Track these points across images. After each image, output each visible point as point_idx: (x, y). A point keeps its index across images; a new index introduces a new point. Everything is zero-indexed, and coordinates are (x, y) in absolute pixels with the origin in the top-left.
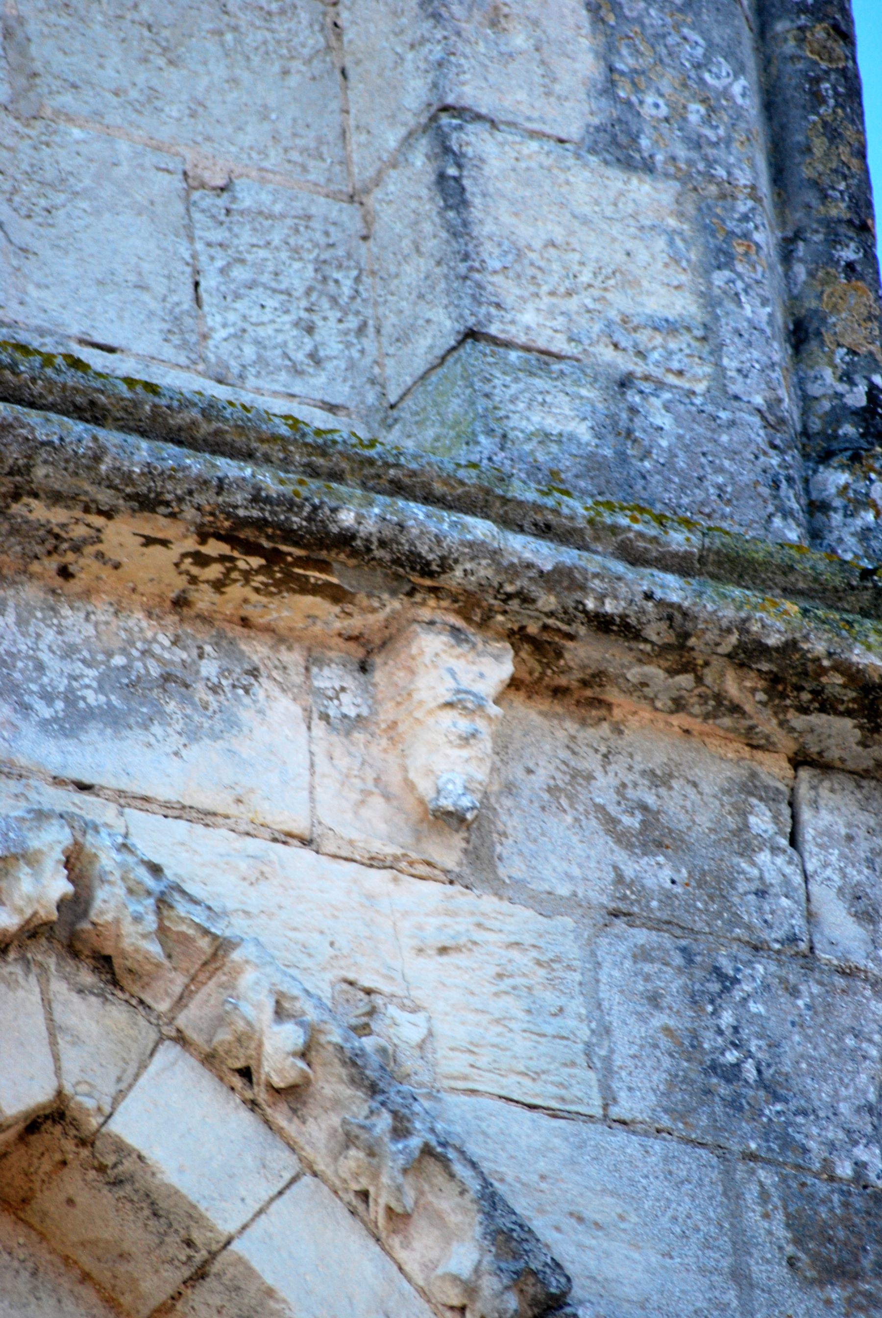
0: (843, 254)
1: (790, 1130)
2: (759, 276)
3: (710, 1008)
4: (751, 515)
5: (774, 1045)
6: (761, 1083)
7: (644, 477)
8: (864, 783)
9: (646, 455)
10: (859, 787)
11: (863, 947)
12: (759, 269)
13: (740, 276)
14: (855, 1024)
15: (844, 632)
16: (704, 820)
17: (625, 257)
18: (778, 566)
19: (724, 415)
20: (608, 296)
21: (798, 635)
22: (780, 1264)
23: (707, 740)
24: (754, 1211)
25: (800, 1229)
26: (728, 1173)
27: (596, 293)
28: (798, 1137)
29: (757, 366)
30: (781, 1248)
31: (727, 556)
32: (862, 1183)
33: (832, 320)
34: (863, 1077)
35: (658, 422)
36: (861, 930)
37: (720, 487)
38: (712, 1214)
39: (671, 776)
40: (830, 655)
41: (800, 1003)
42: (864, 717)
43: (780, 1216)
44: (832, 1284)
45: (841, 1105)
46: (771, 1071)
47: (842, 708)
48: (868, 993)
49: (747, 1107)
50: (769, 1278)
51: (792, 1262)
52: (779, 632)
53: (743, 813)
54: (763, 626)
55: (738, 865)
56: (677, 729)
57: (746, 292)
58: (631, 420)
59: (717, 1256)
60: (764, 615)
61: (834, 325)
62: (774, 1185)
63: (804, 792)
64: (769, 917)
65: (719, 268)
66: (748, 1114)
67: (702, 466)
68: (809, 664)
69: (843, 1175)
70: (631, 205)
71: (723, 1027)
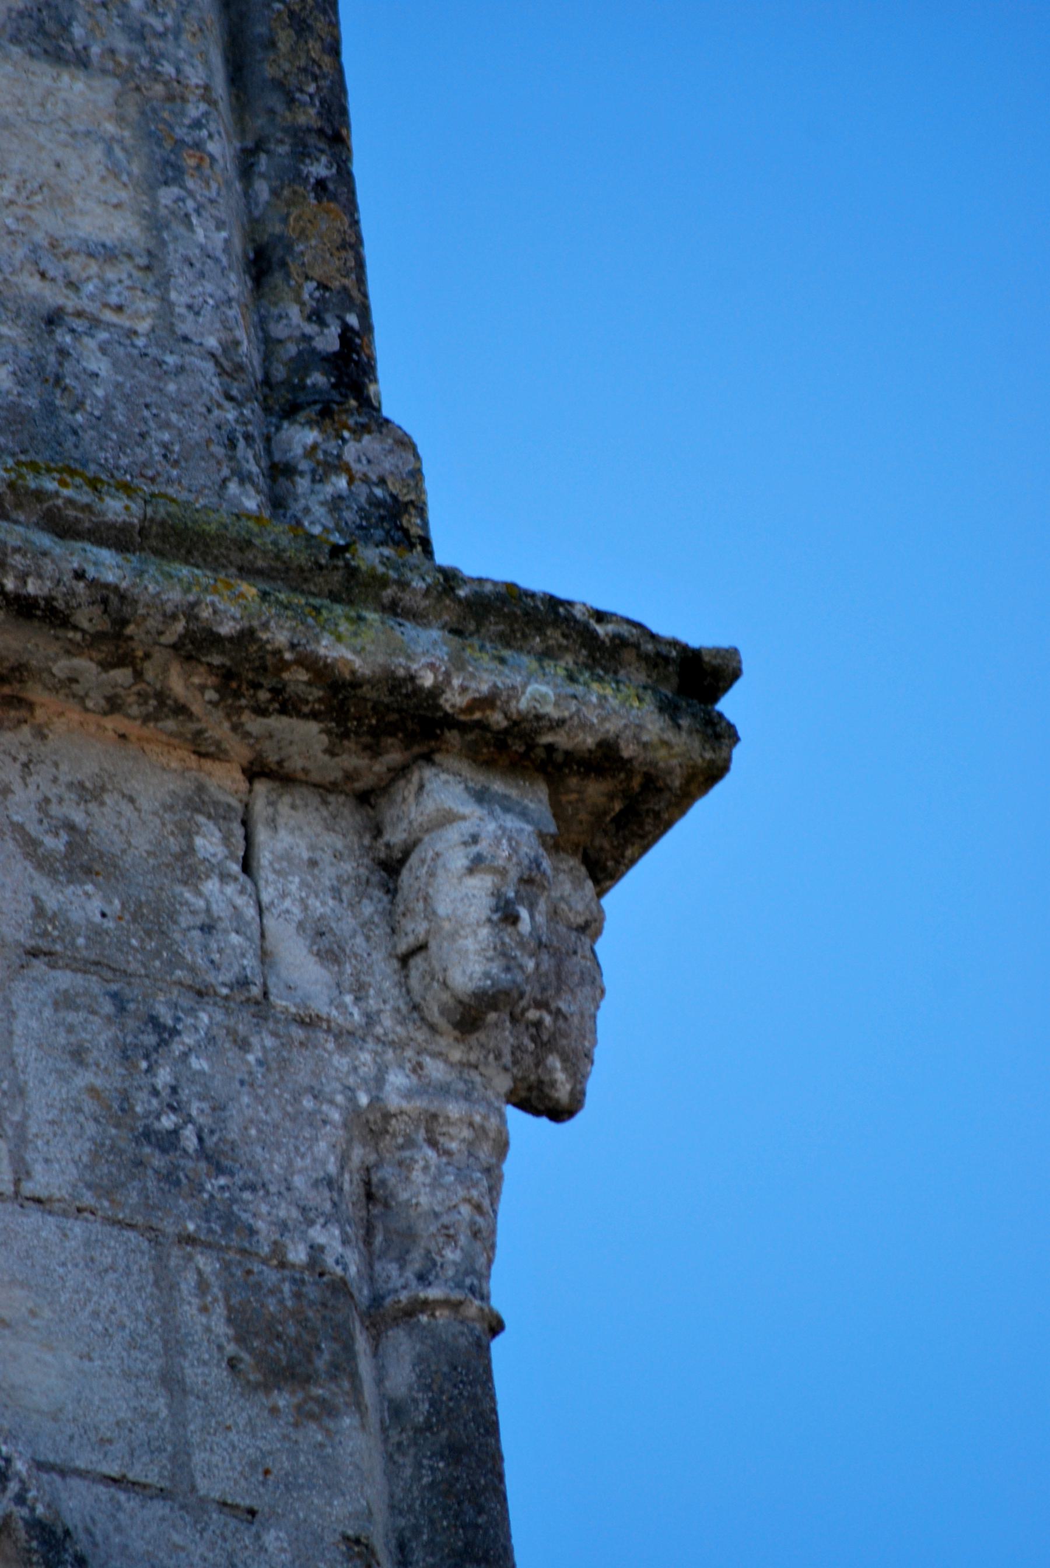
1: (235, 1208)
3: (144, 1065)
4: (202, 480)
5: (219, 1108)
6: (203, 1152)
7: (75, 433)
8: (331, 798)
9: (78, 406)
10: (325, 802)
12: (214, 186)
13: (191, 194)
16: (141, 842)
17: (54, 169)
18: (234, 541)
19: (171, 360)
20: (34, 214)
21: (255, 623)
23: (147, 747)
24: (190, 1303)
27: (19, 211)
28: (244, 1216)
30: (220, 1348)
32: (318, 1270)
33: (299, 247)
37: (165, 446)
39: (103, 789)
40: (293, 646)
41: (251, 1058)
42: (332, 720)
43: (220, 1309)
46: (215, 1138)
47: (306, 709)
48: (331, 1046)
49: (184, 1181)
50: (205, 1383)
51: (233, 1364)
52: (234, 618)
53: (188, 833)
54: (215, 612)
55: (181, 894)
56: (111, 733)
57: (198, 212)
58: (61, 364)
59: (145, 1357)
60: (216, 599)
62: (214, 1272)
63: (260, 808)
64: (216, 957)
65: (166, 183)
67: (145, 421)
68: (268, 657)
69: (297, 1261)
70: (61, 106)
71: (159, 1087)
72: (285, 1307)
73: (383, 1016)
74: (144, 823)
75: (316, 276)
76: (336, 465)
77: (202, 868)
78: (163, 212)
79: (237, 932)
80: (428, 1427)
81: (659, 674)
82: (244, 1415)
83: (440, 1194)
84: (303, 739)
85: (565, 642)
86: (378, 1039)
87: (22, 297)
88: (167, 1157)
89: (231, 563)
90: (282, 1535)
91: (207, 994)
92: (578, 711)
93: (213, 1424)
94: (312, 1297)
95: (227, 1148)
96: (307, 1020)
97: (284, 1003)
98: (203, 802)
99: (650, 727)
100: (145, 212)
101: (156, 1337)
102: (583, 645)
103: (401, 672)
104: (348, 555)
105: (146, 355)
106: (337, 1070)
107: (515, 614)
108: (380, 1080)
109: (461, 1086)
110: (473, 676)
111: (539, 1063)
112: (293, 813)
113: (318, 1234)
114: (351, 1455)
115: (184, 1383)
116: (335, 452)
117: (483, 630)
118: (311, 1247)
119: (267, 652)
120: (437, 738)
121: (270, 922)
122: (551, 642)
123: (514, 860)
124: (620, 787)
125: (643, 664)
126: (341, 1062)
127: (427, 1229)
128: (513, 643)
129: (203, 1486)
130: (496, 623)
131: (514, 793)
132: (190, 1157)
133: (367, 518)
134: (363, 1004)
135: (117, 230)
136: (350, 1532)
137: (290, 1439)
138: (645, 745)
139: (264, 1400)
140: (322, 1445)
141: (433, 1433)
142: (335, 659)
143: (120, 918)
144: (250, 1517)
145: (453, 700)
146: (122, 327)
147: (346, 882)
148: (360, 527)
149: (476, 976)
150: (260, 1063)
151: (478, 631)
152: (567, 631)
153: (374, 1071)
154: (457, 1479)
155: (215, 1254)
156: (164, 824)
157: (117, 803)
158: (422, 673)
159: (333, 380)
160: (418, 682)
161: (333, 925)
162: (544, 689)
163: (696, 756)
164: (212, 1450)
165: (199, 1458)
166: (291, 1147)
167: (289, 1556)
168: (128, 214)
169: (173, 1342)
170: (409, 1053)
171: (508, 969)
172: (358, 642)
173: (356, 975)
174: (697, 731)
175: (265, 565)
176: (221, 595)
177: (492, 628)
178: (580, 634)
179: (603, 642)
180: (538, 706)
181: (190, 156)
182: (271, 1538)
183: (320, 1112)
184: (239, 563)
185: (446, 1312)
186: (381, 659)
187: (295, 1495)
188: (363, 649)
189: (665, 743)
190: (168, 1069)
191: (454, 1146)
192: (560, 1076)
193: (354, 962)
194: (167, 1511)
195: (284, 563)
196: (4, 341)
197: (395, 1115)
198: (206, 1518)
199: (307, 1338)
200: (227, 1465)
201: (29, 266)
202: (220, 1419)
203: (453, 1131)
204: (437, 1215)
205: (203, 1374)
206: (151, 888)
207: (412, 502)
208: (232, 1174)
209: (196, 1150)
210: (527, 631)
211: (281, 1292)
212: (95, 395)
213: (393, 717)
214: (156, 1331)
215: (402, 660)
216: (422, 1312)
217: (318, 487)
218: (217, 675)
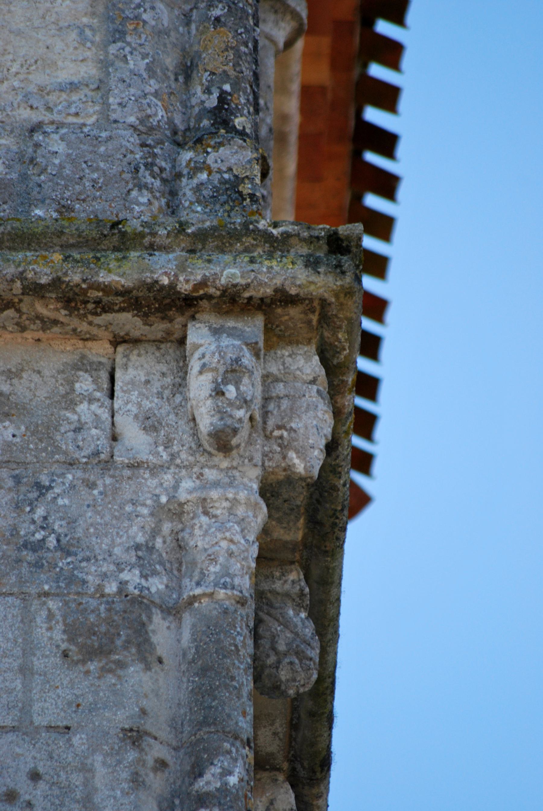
0: (214, 13)
1: (75, 572)
2: (143, 41)
3: (28, 509)
4: (115, 193)
5: (72, 522)
6: (59, 546)
7: (40, 186)
8: (163, 346)
9: (44, 171)
10: (159, 349)
11: (148, 447)
12: (143, 36)
13: (129, 44)
14: (134, 497)
15: (92, 265)
16: (42, 393)
17: (45, 50)
18: (53, 233)
19: (104, 134)
20: (30, 77)
21: (60, 274)
22: (55, 656)
23: (52, 343)
24: (41, 628)
25: (72, 632)
26: (26, 608)
27: (21, 77)
28: (80, 575)
29: (133, 98)
30: (58, 646)
31: (16, 234)
32: (124, 594)
33: (204, 55)
34: (135, 528)
35: (55, 149)
36: (148, 438)
37: (94, 181)
38: (10, 636)
39: (22, 370)
40: (84, 281)
41: (95, 492)
42: (133, 310)
43: (60, 627)
44: (91, 661)
45: (116, 549)
46: (67, 539)
47: (116, 308)
48: (147, 475)
49: (46, 564)
50: (46, 667)
51: (65, 655)
52: (46, 274)
53: (71, 383)
54: (35, 274)
55: (65, 415)
56: (31, 340)
57: (131, 53)
58: (35, 152)
59: (11, 660)
60: (35, 267)
61: (204, 59)
62: (59, 609)
63: (119, 360)
64: (81, 443)
65: (114, 42)
66: (47, 569)
67: (83, 170)
68: (75, 289)
69: (111, 592)
70: (54, 16)
71: (36, 519)
72: (101, 617)
73: (181, 453)
74: (45, 383)
75: (209, 69)
76: (205, 167)
77: (78, 399)
78: (111, 57)
79: (96, 428)
80: (193, 661)
81: (315, 246)
82: (68, 679)
83: (207, 539)
84: (127, 321)
85: (255, 242)
86: (178, 466)
87: (16, 122)
88: (36, 554)
89: (55, 244)
90: (83, 736)
91: (74, 464)
92: (256, 277)
93: (47, 687)
94: (118, 609)
95: (75, 542)
96: (136, 464)
97: (121, 459)
98: (83, 364)
99: (300, 276)
100: (101, 60)
101: (19, 649)
102: (265, 242)
103: (149, 280)
104: (120, 226)
105: (88, 135)
106: (149, 487)
107: (222, 234)
108: (176, 487)
109: (227, 480)
110: (191, 273)
111: (284, 458)
112: (139, 358)
113: (125, 576)
114: (132, 686)
115: (33, 669)
116: (202, 161)
117: (207, 247)
118: (120, 583)
119: (72, 286)
120: (195, 306)
121: (117, 418)
122: (247, 244)
123: (222, 362)
124: (307, 308)
125: (304, 244)
126: (152, 483)
127: (201, 558)
128: (225, 249)
129: (38, 720)
130: (213, 242)
131: (240, 325)
132: (52, 551)
133: (217, 191)
134: (169, 450)
135: (82, 73)
136: (127, 726)
137: (95, 685)
138: (299, 286)
139: (82, 669)
140: (114, 685)
141: (195, 664)
142: (110, 282)
143: (24, 435)
144: (67, 731)
145: (184, 287)
146: (78, 124)
147: (167, 388)
148: (213, 197)
149: (207, 425)
150: (101, 493)
151: (204, 248)
152: (254, 237)
153: (173, 482)
154: (203, 685)
155: (59, 599)
156: (57, 381)
157: (30, 376)
158: (160, 278)
159: (212, 122)
160: (161, 283)
161: (156, 412)
162: (233, 271)
163: (331, 285)
164: (45, 701)
165: (36, 707)
166: (114, 533)
167: (86, 746)
168: (90, 63)
169: (28, 649)
170: (196, 469)
171: (222, 419)
172: (121, 271)
173: (167, 436)
174: (330, 272)
175: (74, 241)
176: (39, 264)
177: (211, 244)
178: (262, 236)
179: (277, 238)
180: (231, 280)
181: (130, 24)
182: (76, 740)
183: (135, 511)
184: (60, 243)
185: (207, 600)
186: (136, 276)
187: (94, 714)
188: (124, 273)
189: (312, 283)
190: (43, 508)
191: (219, 512)
192: (296, 461)
193: (166, 429)
194: (15, 737)
195: (84, 238)
196: (2, 147)
197: (185, 503)
198: (38, 736)
199: (112, 630)
200: (54, 706)
201: (23, 105)
202: (52, 683)
203: (217, 505)
204: (206, 550)
205: (44, 662)
206: (46, 416)
207: (247, 177)
208: (76, 555)
209: (55, 547)
210: (231, 241)
211: (99, 610)
212: (54, 164)
213: (168, 301)
214: (19, 646)
215: (148, 274)
216: (195, 602)
217: (190, 181)
218: (62, 302)
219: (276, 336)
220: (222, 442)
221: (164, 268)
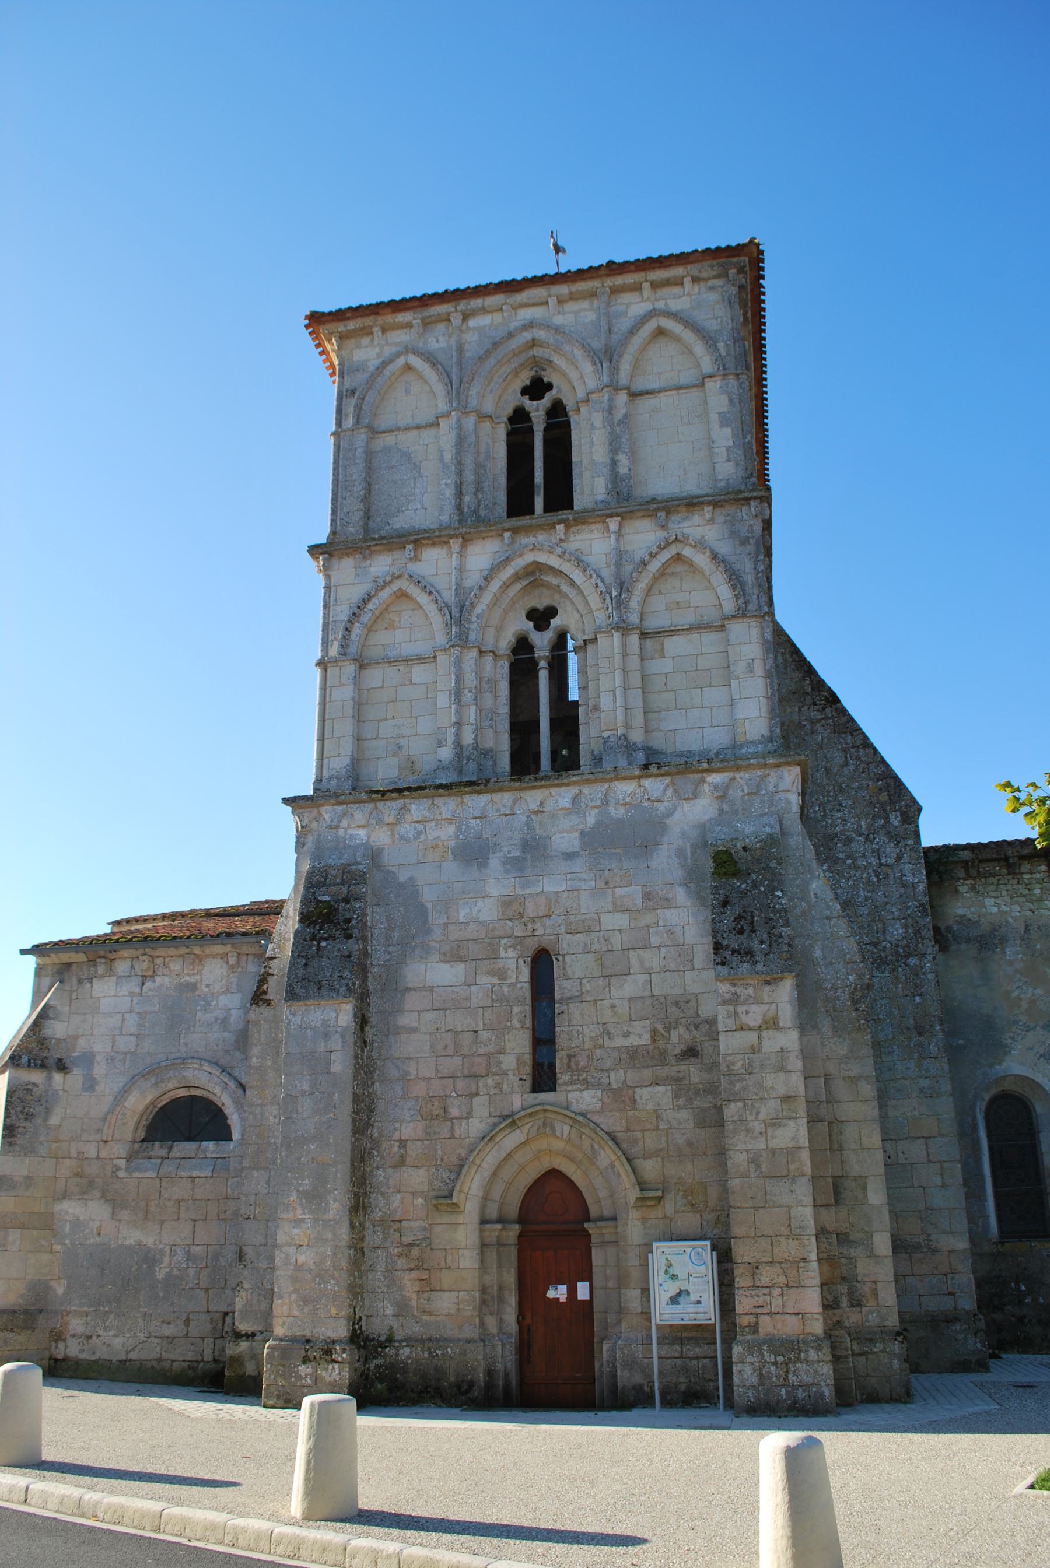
219: (761, 502)
220: (756, 516)
221: (747, 495)
